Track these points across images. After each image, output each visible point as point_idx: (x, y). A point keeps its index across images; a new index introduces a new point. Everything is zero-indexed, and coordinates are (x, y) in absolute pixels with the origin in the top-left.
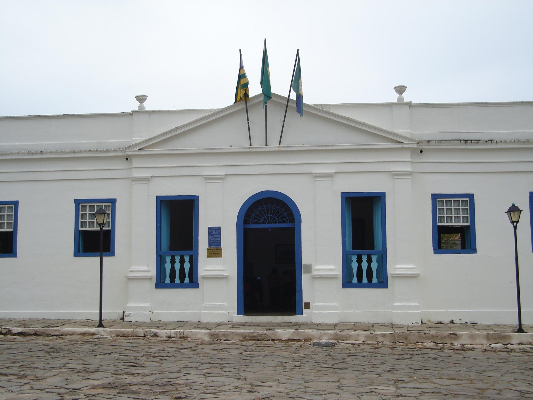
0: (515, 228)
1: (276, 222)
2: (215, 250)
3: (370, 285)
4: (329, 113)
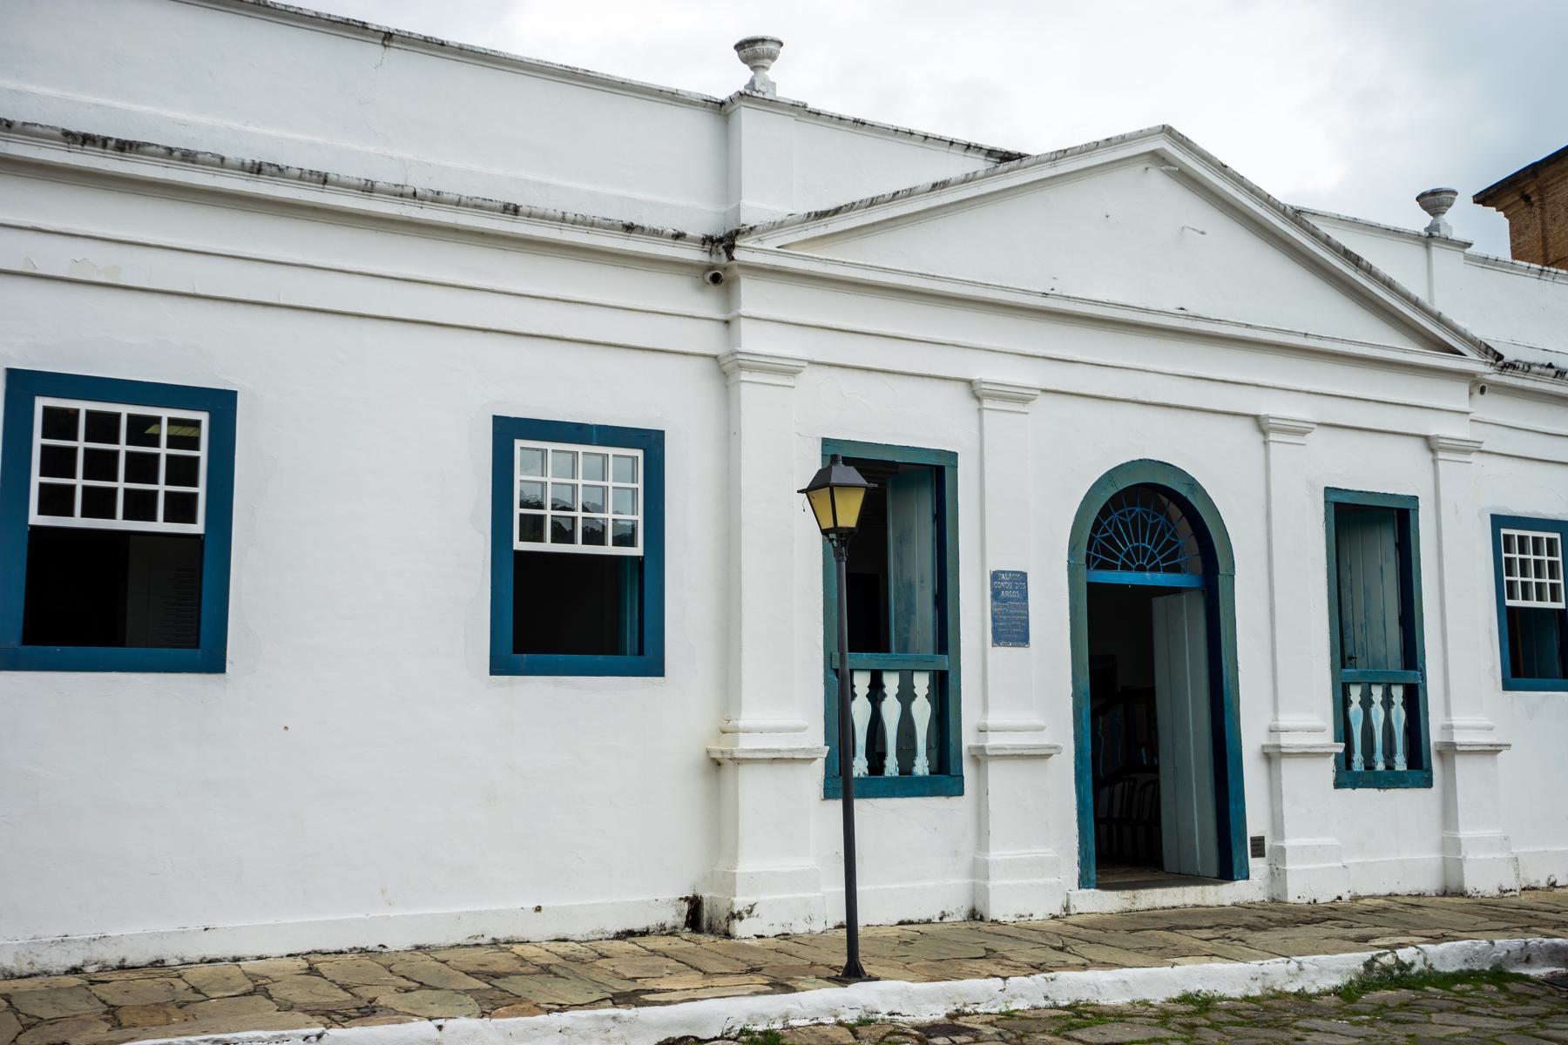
1: (1155, 569)
4: (1314, 234)
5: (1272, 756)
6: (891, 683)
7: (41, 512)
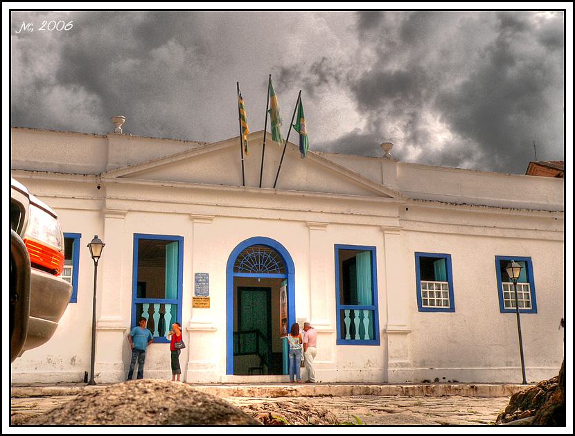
0: (96, 264)
1: (266, 272)
2: (201, 300)
3: (362, 342)
5: (385, 331)
6: (357, 313)
7: (564, 425)
